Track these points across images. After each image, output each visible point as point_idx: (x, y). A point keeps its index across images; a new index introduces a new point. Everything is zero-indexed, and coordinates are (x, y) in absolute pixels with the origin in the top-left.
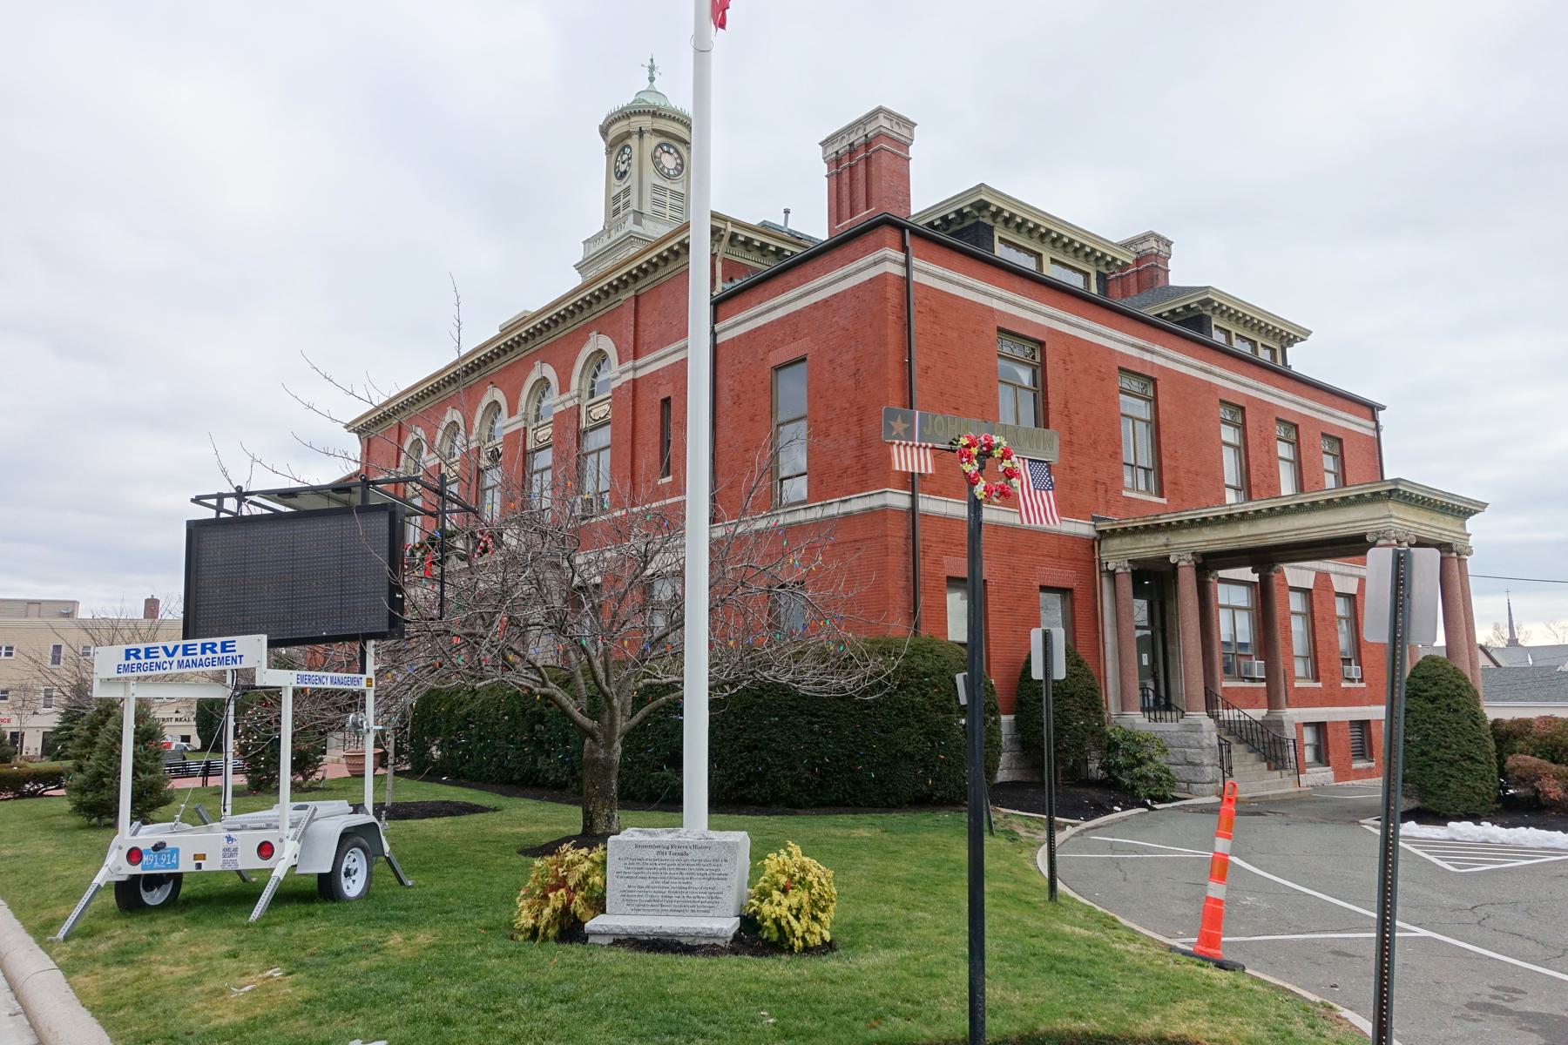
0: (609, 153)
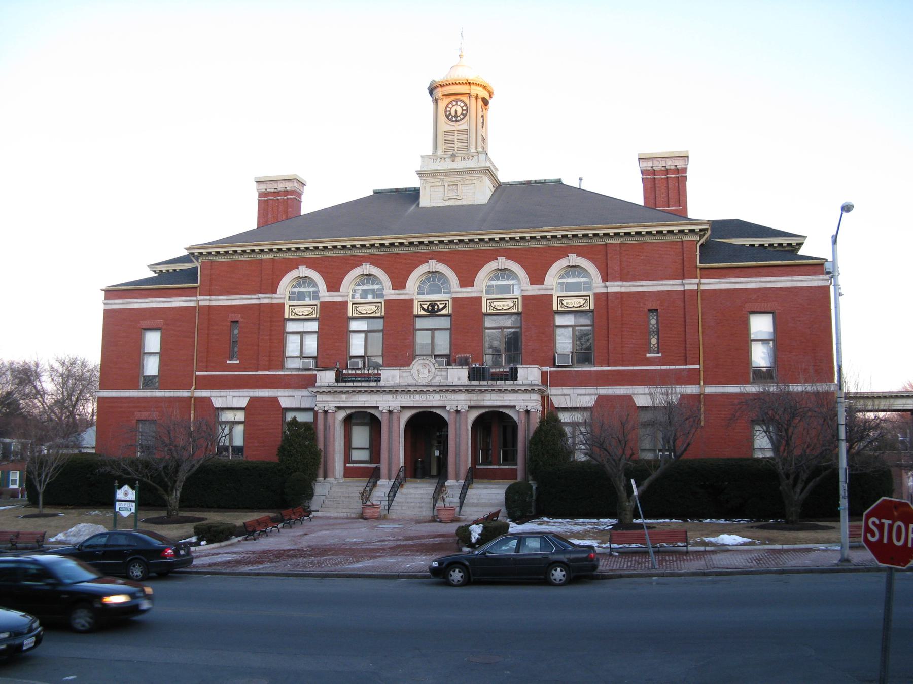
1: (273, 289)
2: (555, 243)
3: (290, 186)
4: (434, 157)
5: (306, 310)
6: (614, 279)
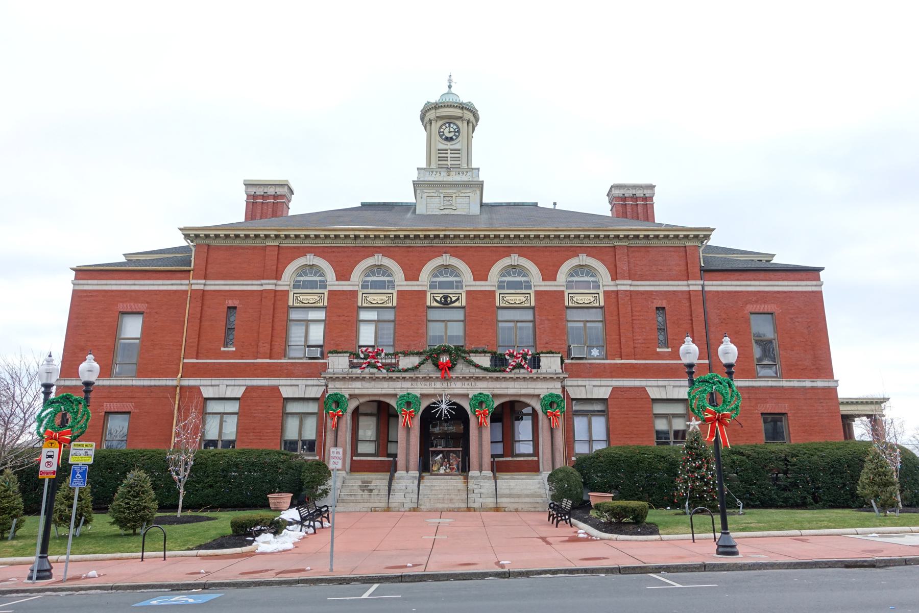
1: (278, 277)
2: (567, 243)
3: (280, 191)
4: (428, 170)
5: (312, 299)
6: (623, 278)
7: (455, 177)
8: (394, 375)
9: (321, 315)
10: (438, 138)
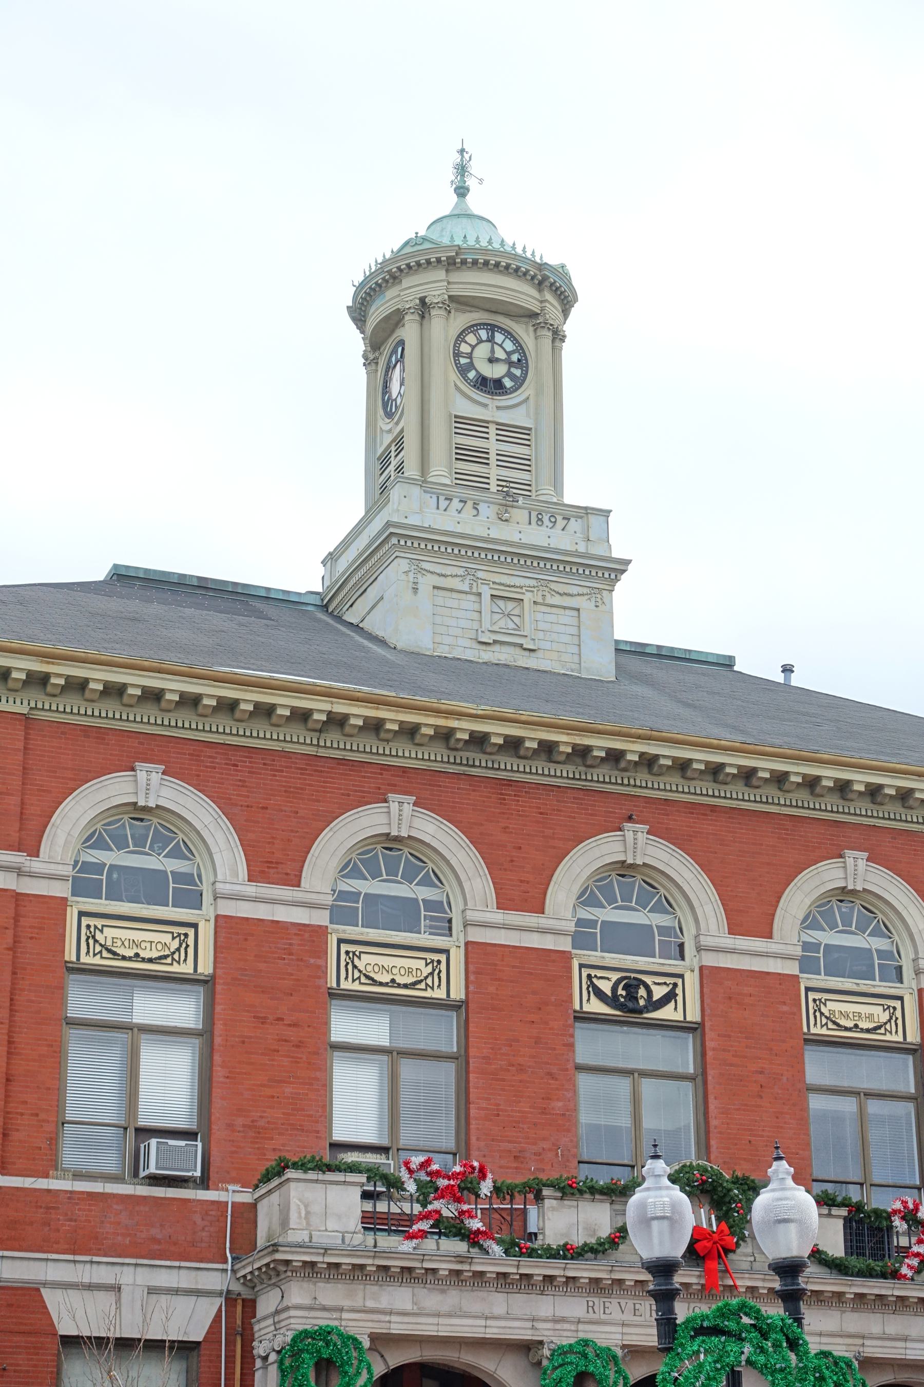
0: (370, 362)
5: (401, 969)
7: (522, 532)
8: (529, 1267)
9: (183, 1010)
10: (454, 376)
